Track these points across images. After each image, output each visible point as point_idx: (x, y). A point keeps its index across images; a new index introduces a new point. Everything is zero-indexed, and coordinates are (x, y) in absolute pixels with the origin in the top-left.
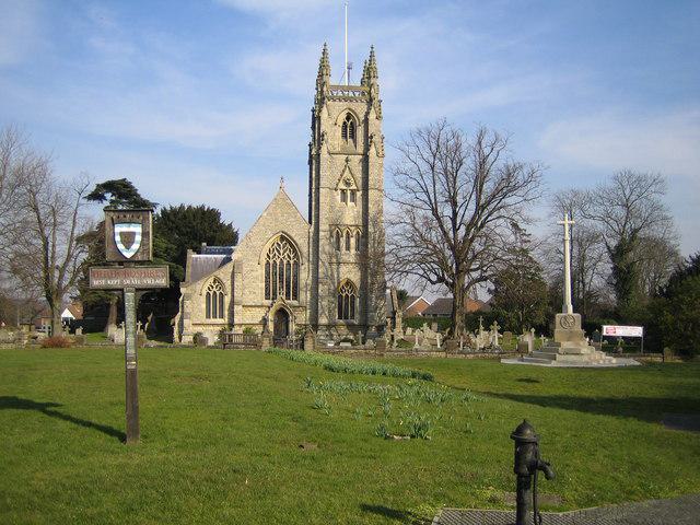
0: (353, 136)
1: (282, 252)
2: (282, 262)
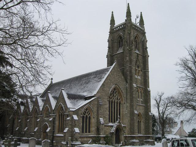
2: (114, 101)
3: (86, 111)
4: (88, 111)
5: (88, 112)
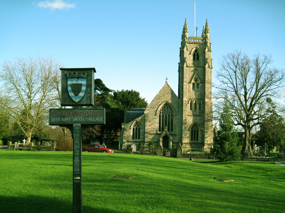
0: (198, 59)
1: (166, 110)
3: (136, 124)
4: (137, 124)
5: (138, 125)
